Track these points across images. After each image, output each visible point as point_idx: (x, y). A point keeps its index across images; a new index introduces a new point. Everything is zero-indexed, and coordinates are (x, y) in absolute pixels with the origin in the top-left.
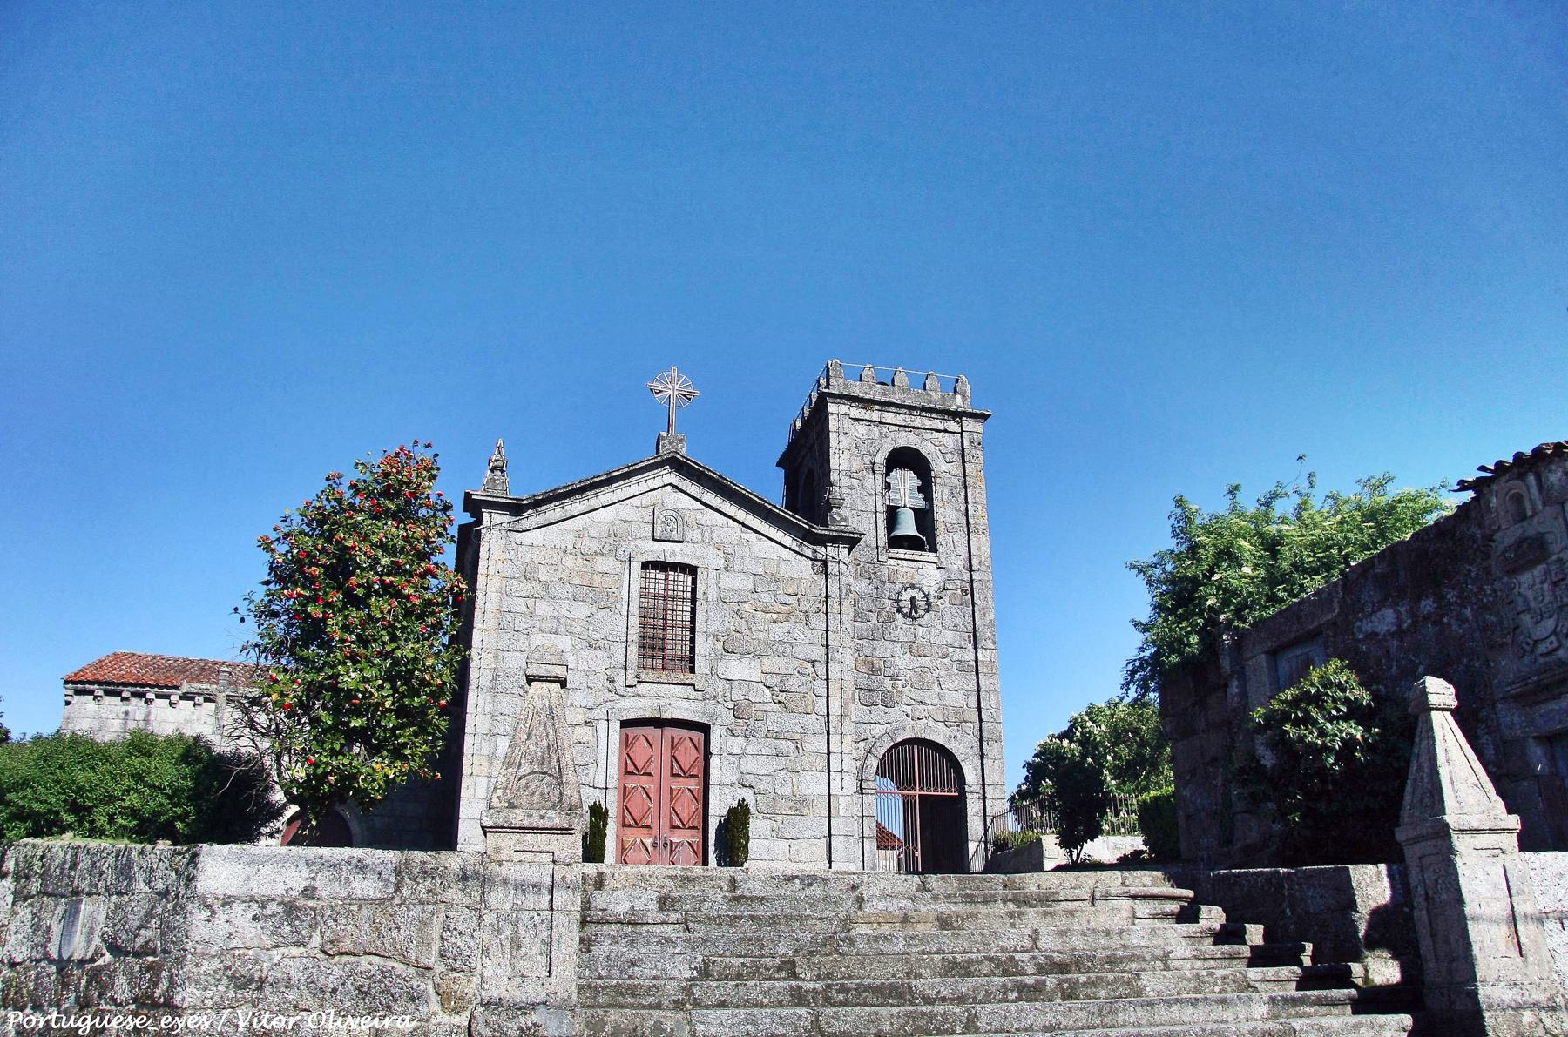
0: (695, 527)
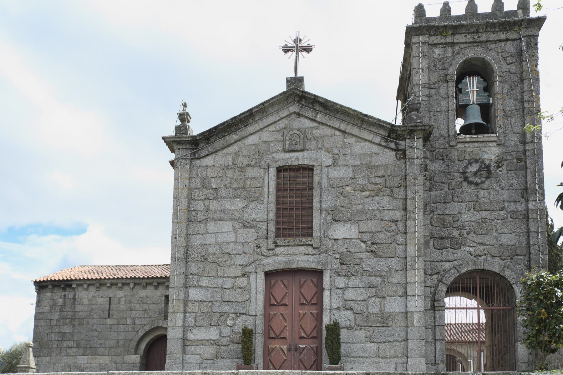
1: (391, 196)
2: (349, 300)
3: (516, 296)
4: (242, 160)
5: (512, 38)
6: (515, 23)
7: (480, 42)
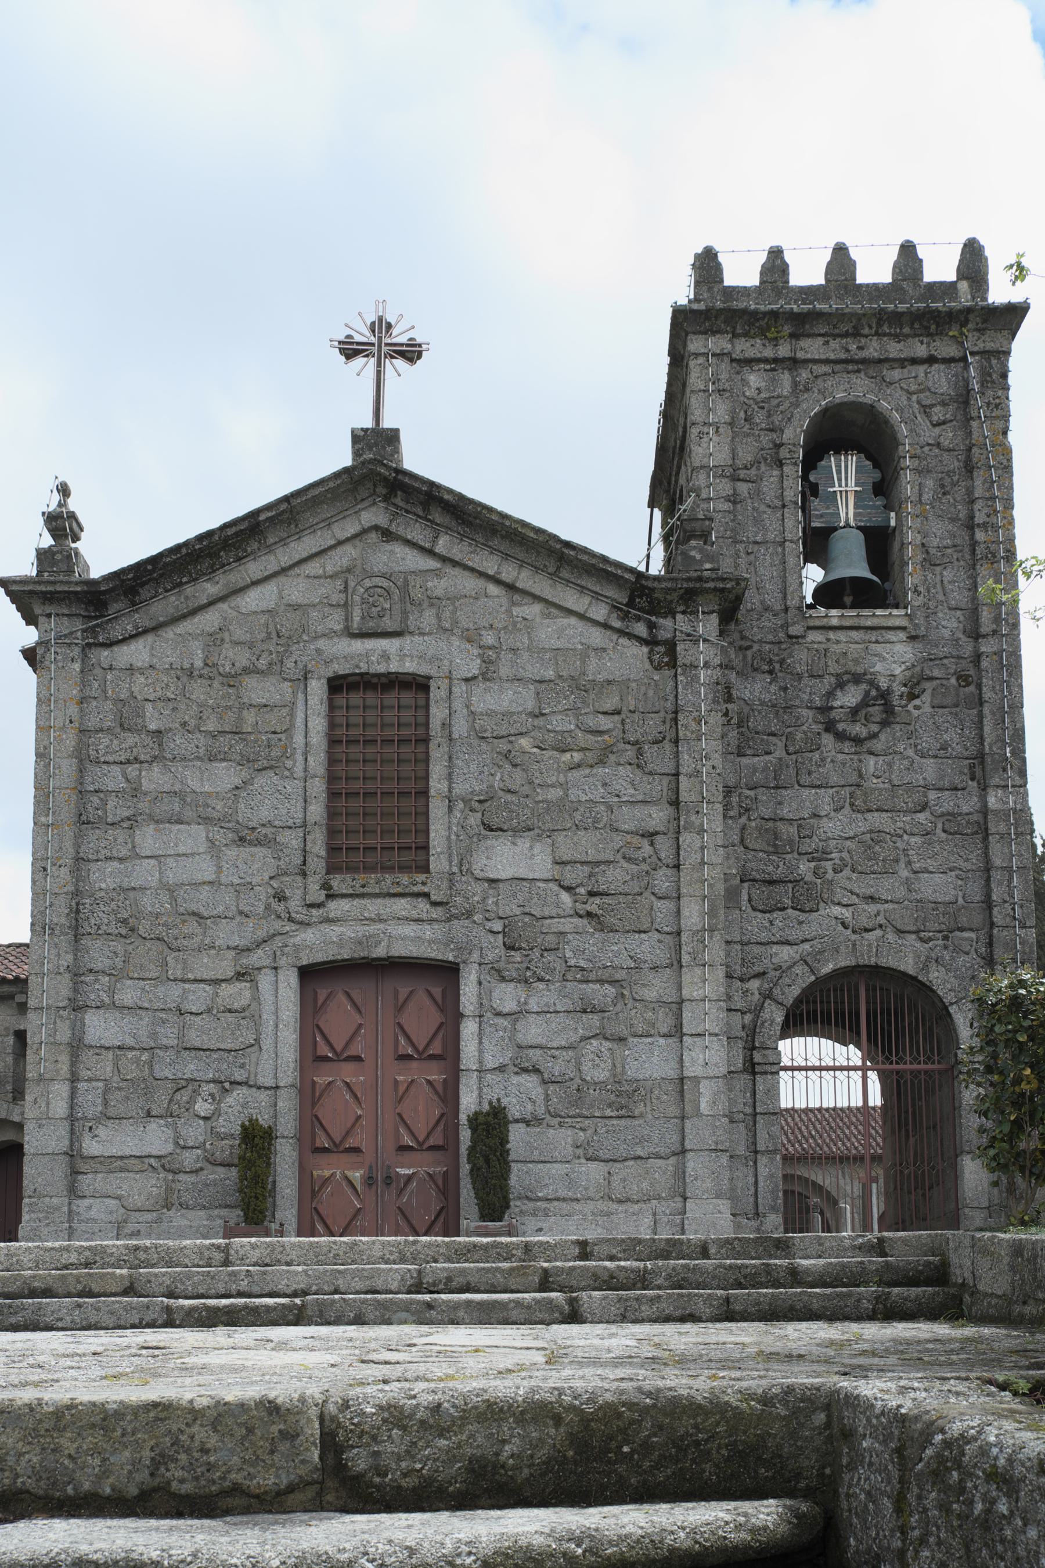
1: (638, 766)
2: (531, 1047)
4: (230, 654)
5: (945, 355)
7: (864, 361)
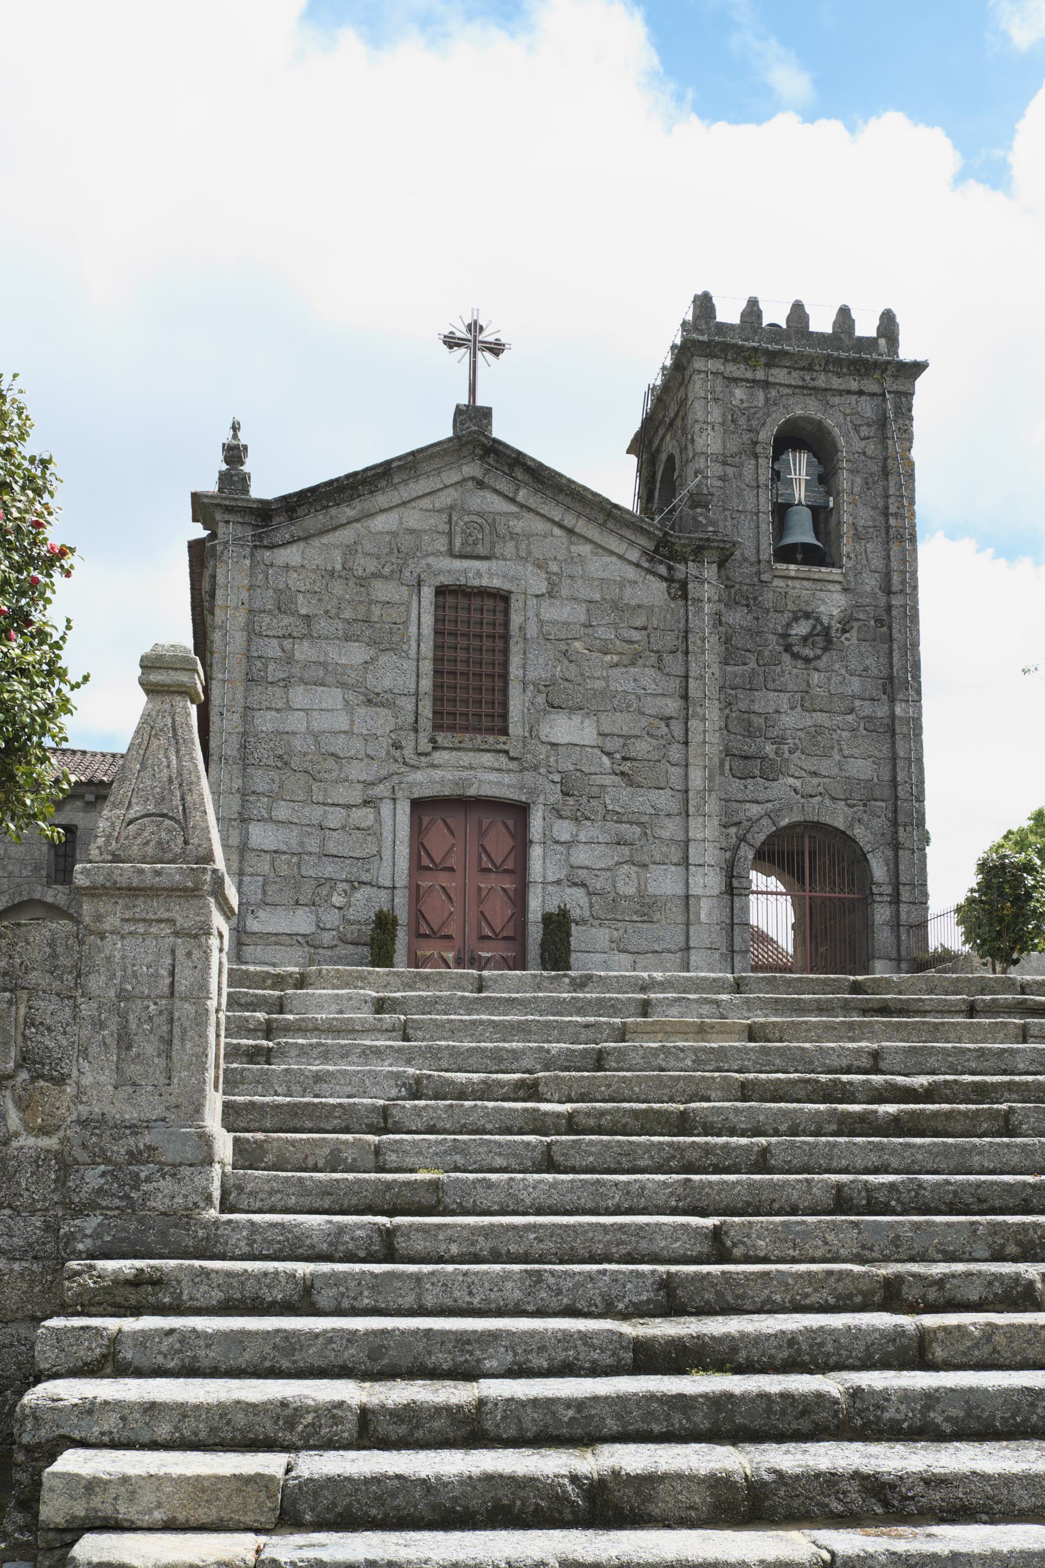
0: (508, 538)
1: (659, 669)
2: (580, 867)
3: (872, 874)
4: (362, 562)
5: (870, 390)
6: (876, 364)
7: (814, 388)
